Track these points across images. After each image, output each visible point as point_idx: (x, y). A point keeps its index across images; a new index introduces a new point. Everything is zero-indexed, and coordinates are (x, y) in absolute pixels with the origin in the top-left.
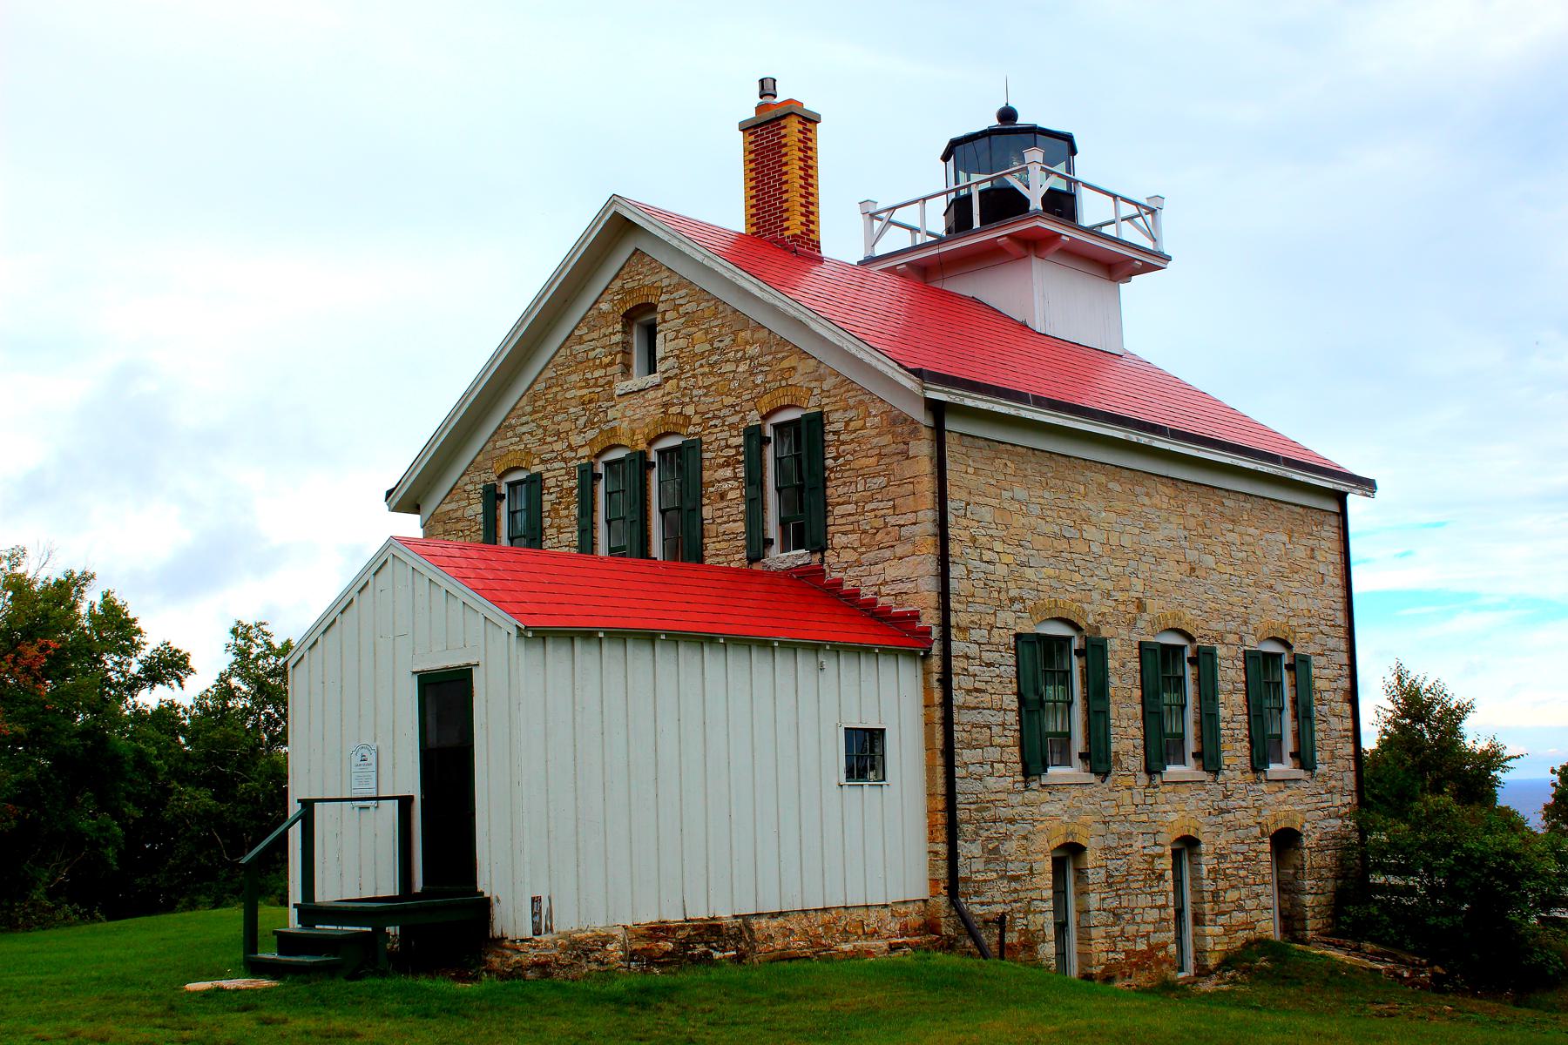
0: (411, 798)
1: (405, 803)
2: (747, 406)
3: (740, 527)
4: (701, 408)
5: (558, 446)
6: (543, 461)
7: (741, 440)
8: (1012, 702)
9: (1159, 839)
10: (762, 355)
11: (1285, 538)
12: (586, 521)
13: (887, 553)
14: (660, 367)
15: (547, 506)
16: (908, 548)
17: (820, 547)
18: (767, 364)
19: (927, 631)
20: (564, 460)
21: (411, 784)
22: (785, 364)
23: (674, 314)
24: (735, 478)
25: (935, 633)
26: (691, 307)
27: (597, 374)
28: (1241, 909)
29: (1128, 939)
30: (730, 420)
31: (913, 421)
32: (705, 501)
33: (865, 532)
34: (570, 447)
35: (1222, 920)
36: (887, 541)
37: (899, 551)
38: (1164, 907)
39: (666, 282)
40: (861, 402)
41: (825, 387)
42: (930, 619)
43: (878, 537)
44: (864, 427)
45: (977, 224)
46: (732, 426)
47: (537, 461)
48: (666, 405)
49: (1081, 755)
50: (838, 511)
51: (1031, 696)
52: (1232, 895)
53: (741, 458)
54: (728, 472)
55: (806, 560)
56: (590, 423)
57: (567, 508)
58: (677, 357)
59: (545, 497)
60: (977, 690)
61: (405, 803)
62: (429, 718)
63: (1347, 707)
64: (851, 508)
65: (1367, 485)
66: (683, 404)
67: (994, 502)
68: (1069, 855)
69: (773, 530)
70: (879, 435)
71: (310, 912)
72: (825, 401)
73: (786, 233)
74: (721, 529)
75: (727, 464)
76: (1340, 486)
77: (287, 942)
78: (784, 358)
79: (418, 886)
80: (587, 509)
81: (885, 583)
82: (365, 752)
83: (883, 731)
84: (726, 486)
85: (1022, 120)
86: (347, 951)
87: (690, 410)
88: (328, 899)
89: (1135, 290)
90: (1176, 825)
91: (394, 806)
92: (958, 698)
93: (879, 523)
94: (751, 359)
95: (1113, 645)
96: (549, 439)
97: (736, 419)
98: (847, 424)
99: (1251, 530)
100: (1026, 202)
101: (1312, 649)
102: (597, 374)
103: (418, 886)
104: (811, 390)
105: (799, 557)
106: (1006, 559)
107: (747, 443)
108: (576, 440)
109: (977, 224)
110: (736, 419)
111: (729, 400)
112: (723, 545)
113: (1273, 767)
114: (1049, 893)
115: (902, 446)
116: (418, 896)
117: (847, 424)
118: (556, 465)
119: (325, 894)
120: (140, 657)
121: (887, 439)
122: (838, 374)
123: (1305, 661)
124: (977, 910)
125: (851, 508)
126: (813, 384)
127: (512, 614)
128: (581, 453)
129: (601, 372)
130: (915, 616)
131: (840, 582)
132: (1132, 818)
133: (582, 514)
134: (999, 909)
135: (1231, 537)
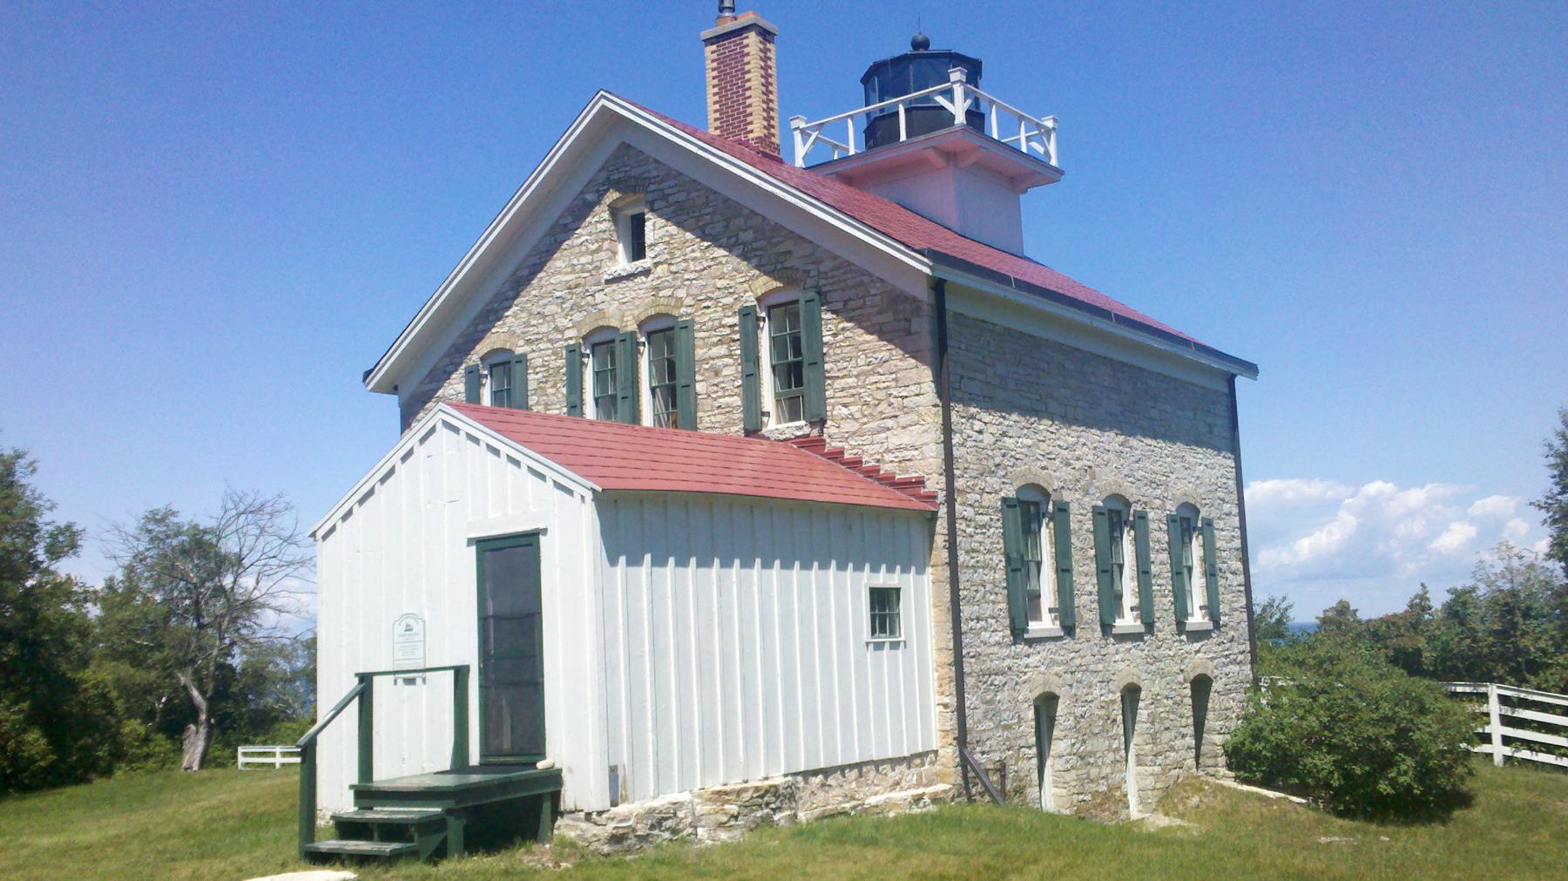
0: (467, 668)
1: (461, 673)
2: (741, 288)
3: (737, 401)
4: (694, 291)
5: (544, 328)
6: (529, 342)
7: (735, 320)
8: (998, 559)
9: (1113, 688)
10: (756, 240)
11: (1191, 415)
12: (573, 398)
13: (890, 423)
14: (649, 253)
15: (532, 385)
16: (915, 417)
17: (821, 422)
18: (761, 249)
19: (932, 497)
20: (550, 341)
21: (470, 655)
22: (781, 248)
23: (663, 203)
24: (730, 356)
25: (941, 496)
26: (681, 197)
27: (583, 260)
28: (1172, 749)
29: (1092, 781)
30: (724, 301)
31: (914, 300)
32: (698, 377)
33: (866, 404)
34: (556, 329)
35: (1160, 760)
36: (889, 411)
37: (903, 420)
38: (1118, 749)
39: (655, 173)
40: (861, 284)
41: (822, 269)
42: (935, 484)
43: (880, 408)
44: (863, 306)
45: (903, 137)
46: (730, 306)
47: (521, 342)
48: (657, 289)
49: (1051, 610)
50: (838, 384)
51: (1014, 555)
52: (1166, 736)
53: (737, 337)
54: (723, 350)
55: (807, 430)
56: (576, 307)
57: (554, 386)
58: (668, 243)
59: (531, 377)
60: (974, 551)
61: (461, 673)
62: (488, 586)
63: (1239, 565)
64: (851, 381)
65: (1251, 369)
66: (676, 288)
67: (980, 376)
68: (1046, 706)
69: (768, 401)
70: (879, 313)
71: (366, 794)
72: (822, 282)
73: (751, 136)
74: (717, 404)
75: (720, 342)
76: (1231, 369)
77: (347, 828)
78: (779, 243)
79: (475, 758)
80: (575, 385)
81: (888, 451)
82: (412, 622)
83: (898, 590)
84: (719, 363)
85: (934, 47)
86: (391, 827)
87: (681, 293)
88: (384, 778)
89: (1033, 201)
90: (1124, 673)
91: (452, 672)
92: (962, 558)
93: (881, 395)
94: (745, 244)
95: (1074, 508)
96: (534, 322)
97: (730, 300)
98: (846, 302)
99: (1168, 408)
100: (952, 117)
101: (1214, 514)
102: (583, 260)
103: (475, 758)
104: (808, 272)
105: (800, 427)
106: (992, 429)
107: (743, 324)
108: (563, 322)
109: (903, 137)
110: (730, 300)
111: (720, 283)
112: (720, 418)
113: (1032, 625)
114: (1033, 740)
115: (903, 323)
116: (474, 770)
117: (846, 302)
118: (542, 346)
119: (385, 774)
120: (42, 544)
121: (889, 316)
122: (836, 257)
123: (1209, 523)
124: (977, 756)
125: (851, 381)
126: (811, 267)
127: (586, 476)
128: (568, 334)
129: (588, 258)
130: (920, 482)
131: (841, 452)
132: (1092, 667)
133: (570, 391)
134: (996, 757)
135: (1154, 413)
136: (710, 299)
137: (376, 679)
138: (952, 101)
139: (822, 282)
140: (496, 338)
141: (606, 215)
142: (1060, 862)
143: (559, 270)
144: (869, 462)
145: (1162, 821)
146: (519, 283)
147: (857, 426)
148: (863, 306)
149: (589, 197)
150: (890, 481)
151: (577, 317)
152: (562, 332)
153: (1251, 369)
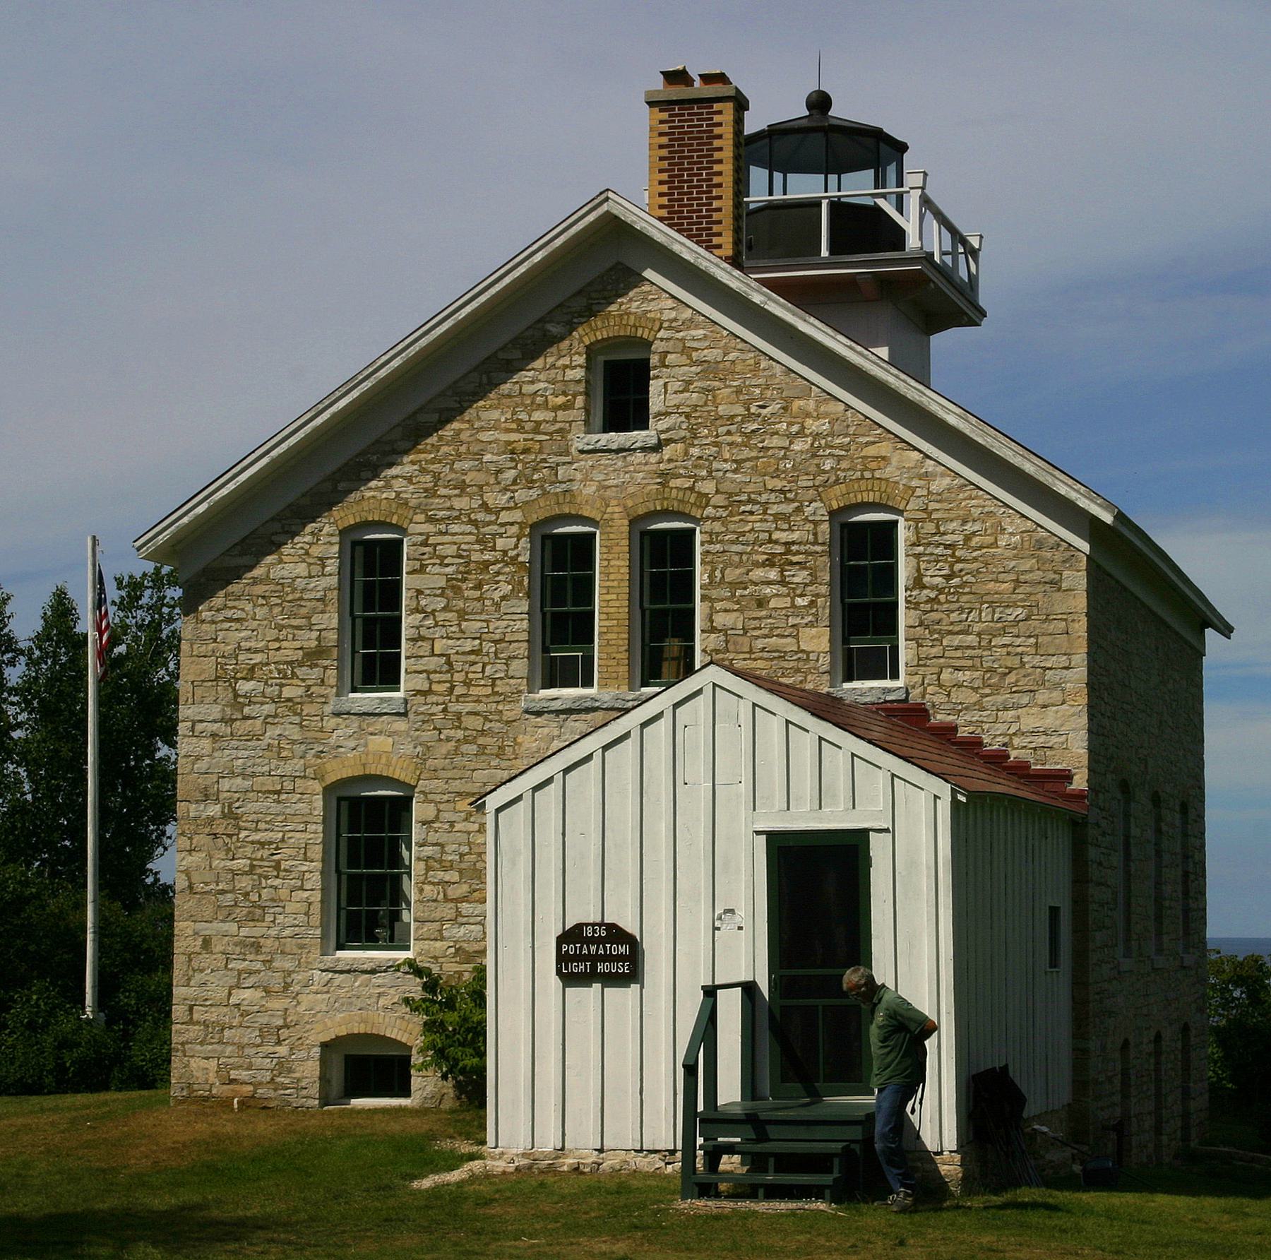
4: (725, 487)
6: (430, 520)
20: (474, 523)
22: (871, 451)
26: (711, 355)
27: (538, 416)
34: (485, 507)
41: (934, 487)
45: (825, 253)
48: (665, 476)
58: (688, 416)
84: (768, 590)
87: (708, 487)
102: (538, 416)
104: (914, 489)
109: (825, 253)
118: (455, 528)
125: (971, 639)
136: (755, 502)
137: (720, 993)
138: (900, 209)
139: (932, 506)
140: (373, 499)
141: (581, 360)
142: (496, 1210)
143: (490, 423)
144: (992, 743)
145: (836, 1170)
146: (415, 433)
147: (975, 697)
148: (994, 544)
149: (554, 329)
150: (1021, 771)
151: (521, 495)
152: (497, 513)
153: (1226, 630)
